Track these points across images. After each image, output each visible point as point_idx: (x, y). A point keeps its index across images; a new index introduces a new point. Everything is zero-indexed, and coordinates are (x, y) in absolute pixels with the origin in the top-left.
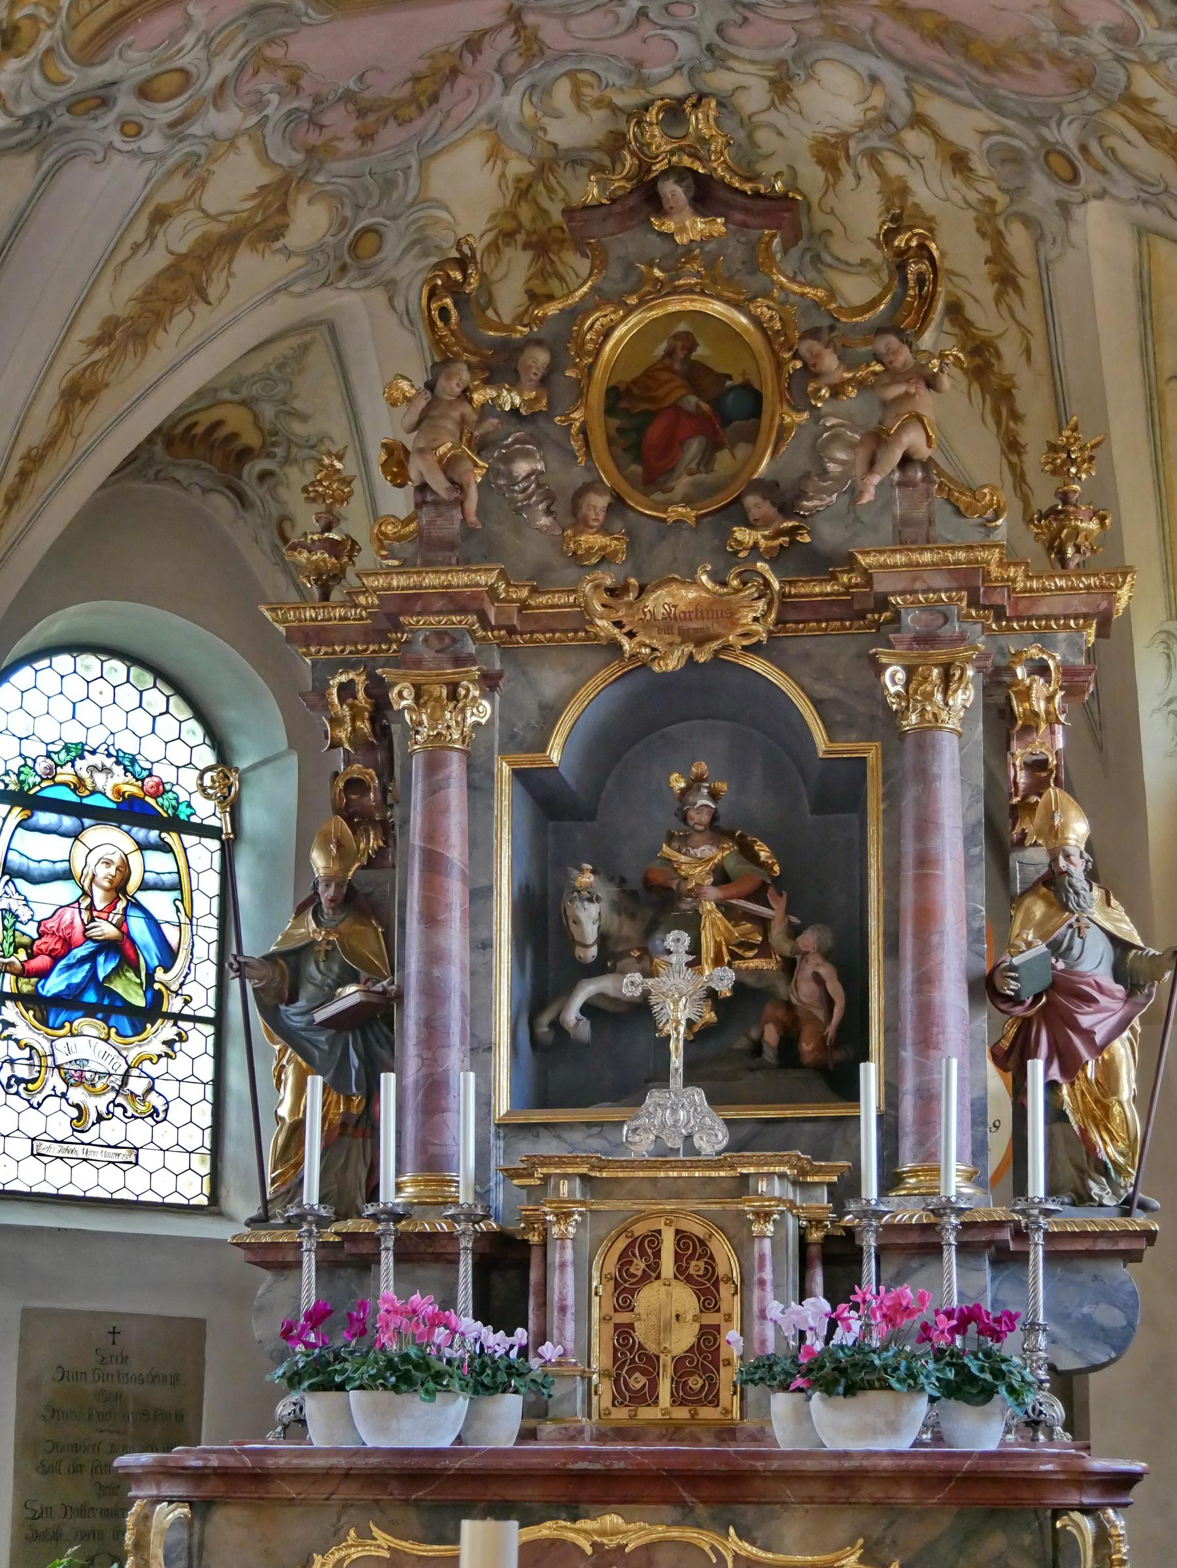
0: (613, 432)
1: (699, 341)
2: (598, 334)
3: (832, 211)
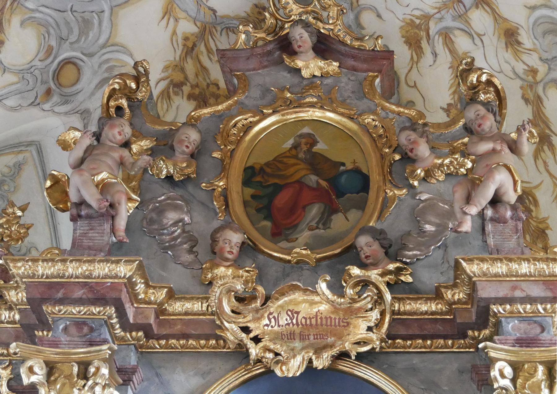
0: (248, 198)
1: (319, 139)
2: (239, 131)
3: (415, 86)
